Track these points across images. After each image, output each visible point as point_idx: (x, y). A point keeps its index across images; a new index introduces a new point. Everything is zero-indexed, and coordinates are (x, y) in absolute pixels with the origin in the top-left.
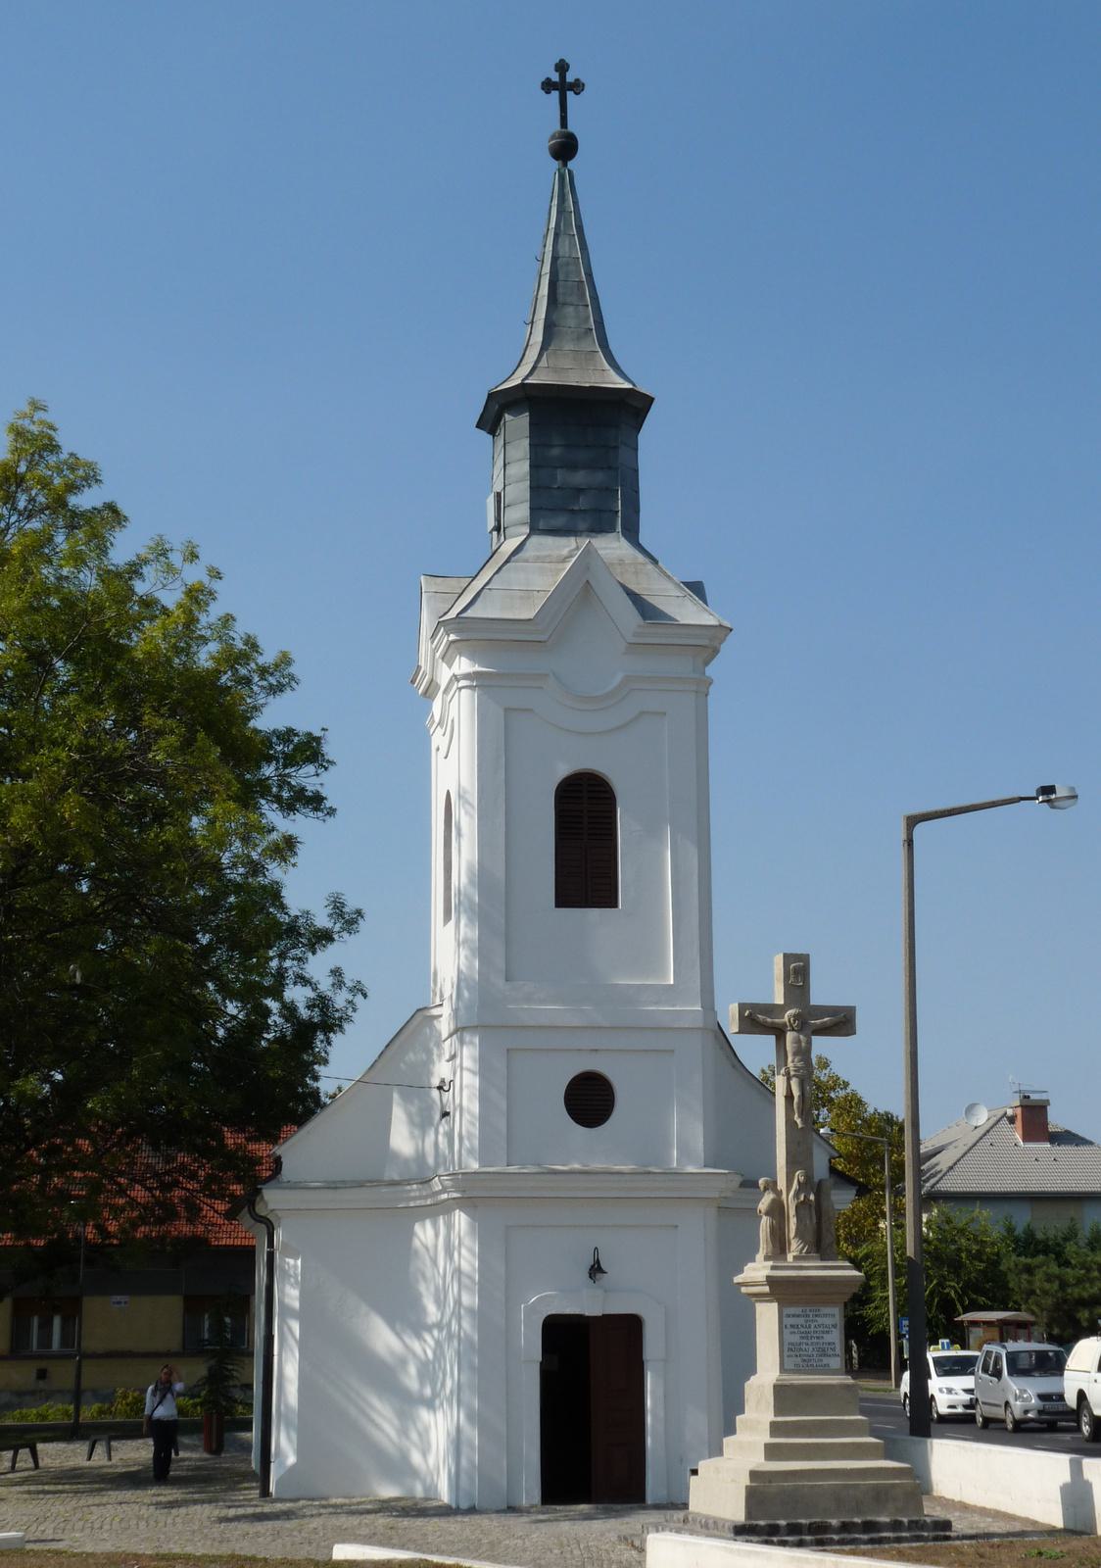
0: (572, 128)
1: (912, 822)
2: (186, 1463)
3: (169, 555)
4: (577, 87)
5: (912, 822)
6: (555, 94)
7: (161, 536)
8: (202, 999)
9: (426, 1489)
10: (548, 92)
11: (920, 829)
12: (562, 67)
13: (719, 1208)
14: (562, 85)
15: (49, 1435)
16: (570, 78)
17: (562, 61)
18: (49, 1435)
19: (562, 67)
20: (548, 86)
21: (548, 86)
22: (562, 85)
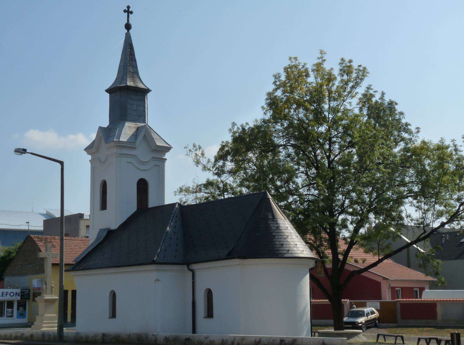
0: (130, 22)
1: (62, 163)
2: (45, 286)
3: (372, 87)
4: (132, 13)
5: (62, 163)
6: (126, 13)
7: (242, 124)
8: (237, 134)
9: (17, 249)
10: (125, 12)
11: (59, 165)
12: (128, 7)
13: (107, 148)
14: (128, 12)
15: (351, 326)
16: (130, 10)
17: (129, 6)
18: (351, 326)
19: (128, 7)
20: (125, 11)
21: (125, 11)
22: (128, 12)
